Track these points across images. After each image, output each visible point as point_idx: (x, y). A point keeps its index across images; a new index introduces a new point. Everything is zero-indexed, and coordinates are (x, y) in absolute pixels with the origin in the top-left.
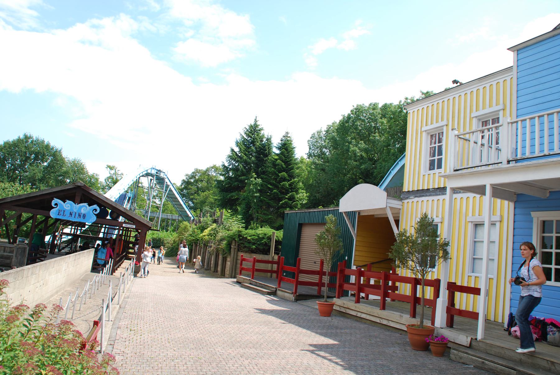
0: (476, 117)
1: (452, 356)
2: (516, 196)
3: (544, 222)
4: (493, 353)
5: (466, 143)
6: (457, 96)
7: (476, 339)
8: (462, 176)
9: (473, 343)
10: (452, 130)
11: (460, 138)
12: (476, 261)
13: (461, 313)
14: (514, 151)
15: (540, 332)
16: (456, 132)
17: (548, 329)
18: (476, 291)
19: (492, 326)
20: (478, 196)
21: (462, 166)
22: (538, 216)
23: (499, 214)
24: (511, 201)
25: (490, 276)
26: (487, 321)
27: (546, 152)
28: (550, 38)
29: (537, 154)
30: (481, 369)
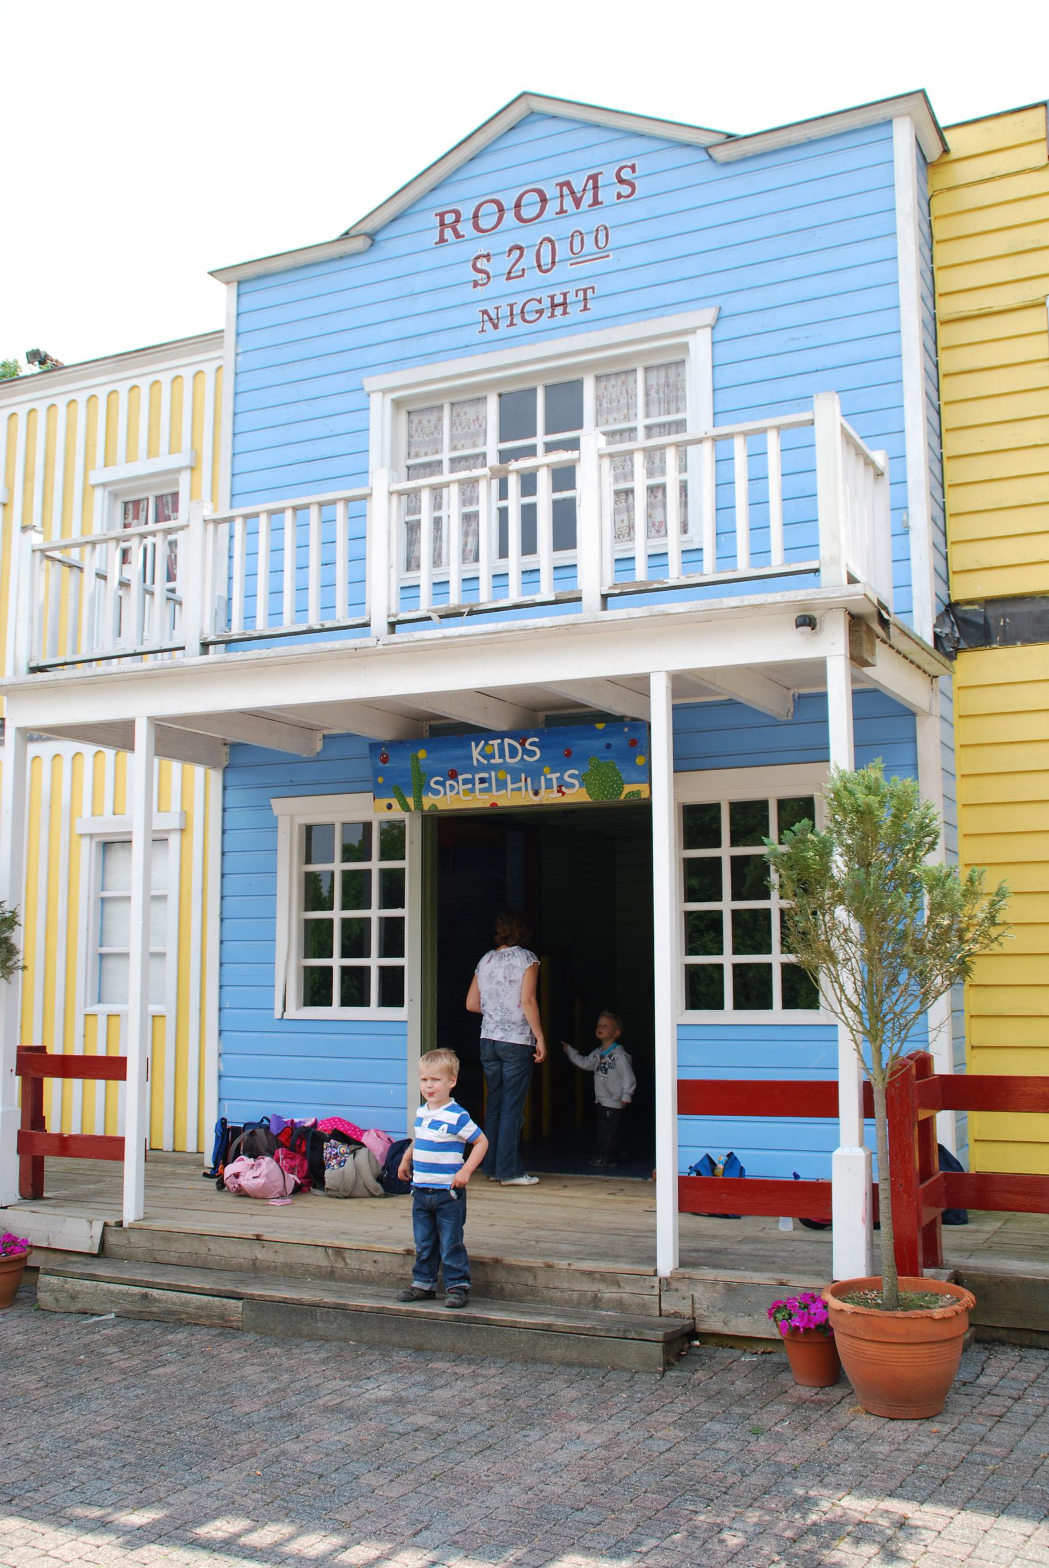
0: (104, 485)
1: (45, 1298)
2: (227, 749)
3: (309, 829)
4: (173, 1258)
5: (72, 576)
6: (42, 407)
7: (120, 1224)
8: (58, 688)
9: (111, 1239)
10: (24, 529)
11: (48, 557)
12: (110, 963)
13: (65, 1145)
14: (223, 606)
15: (306, 1164)
16: (36, 539)
17: (326, 1153)
18: (112, 1068)
19: (168, 1169)
20: (109, 753)
21: (54, 655)
22: (294, 812)
23: (179, 810)
24: (214, 767)
25: (154, 1008)
26: (151, 1154)
27: (313, 620)
28: (332, 260)
29: (287, 624)
30: (140, 1317)
